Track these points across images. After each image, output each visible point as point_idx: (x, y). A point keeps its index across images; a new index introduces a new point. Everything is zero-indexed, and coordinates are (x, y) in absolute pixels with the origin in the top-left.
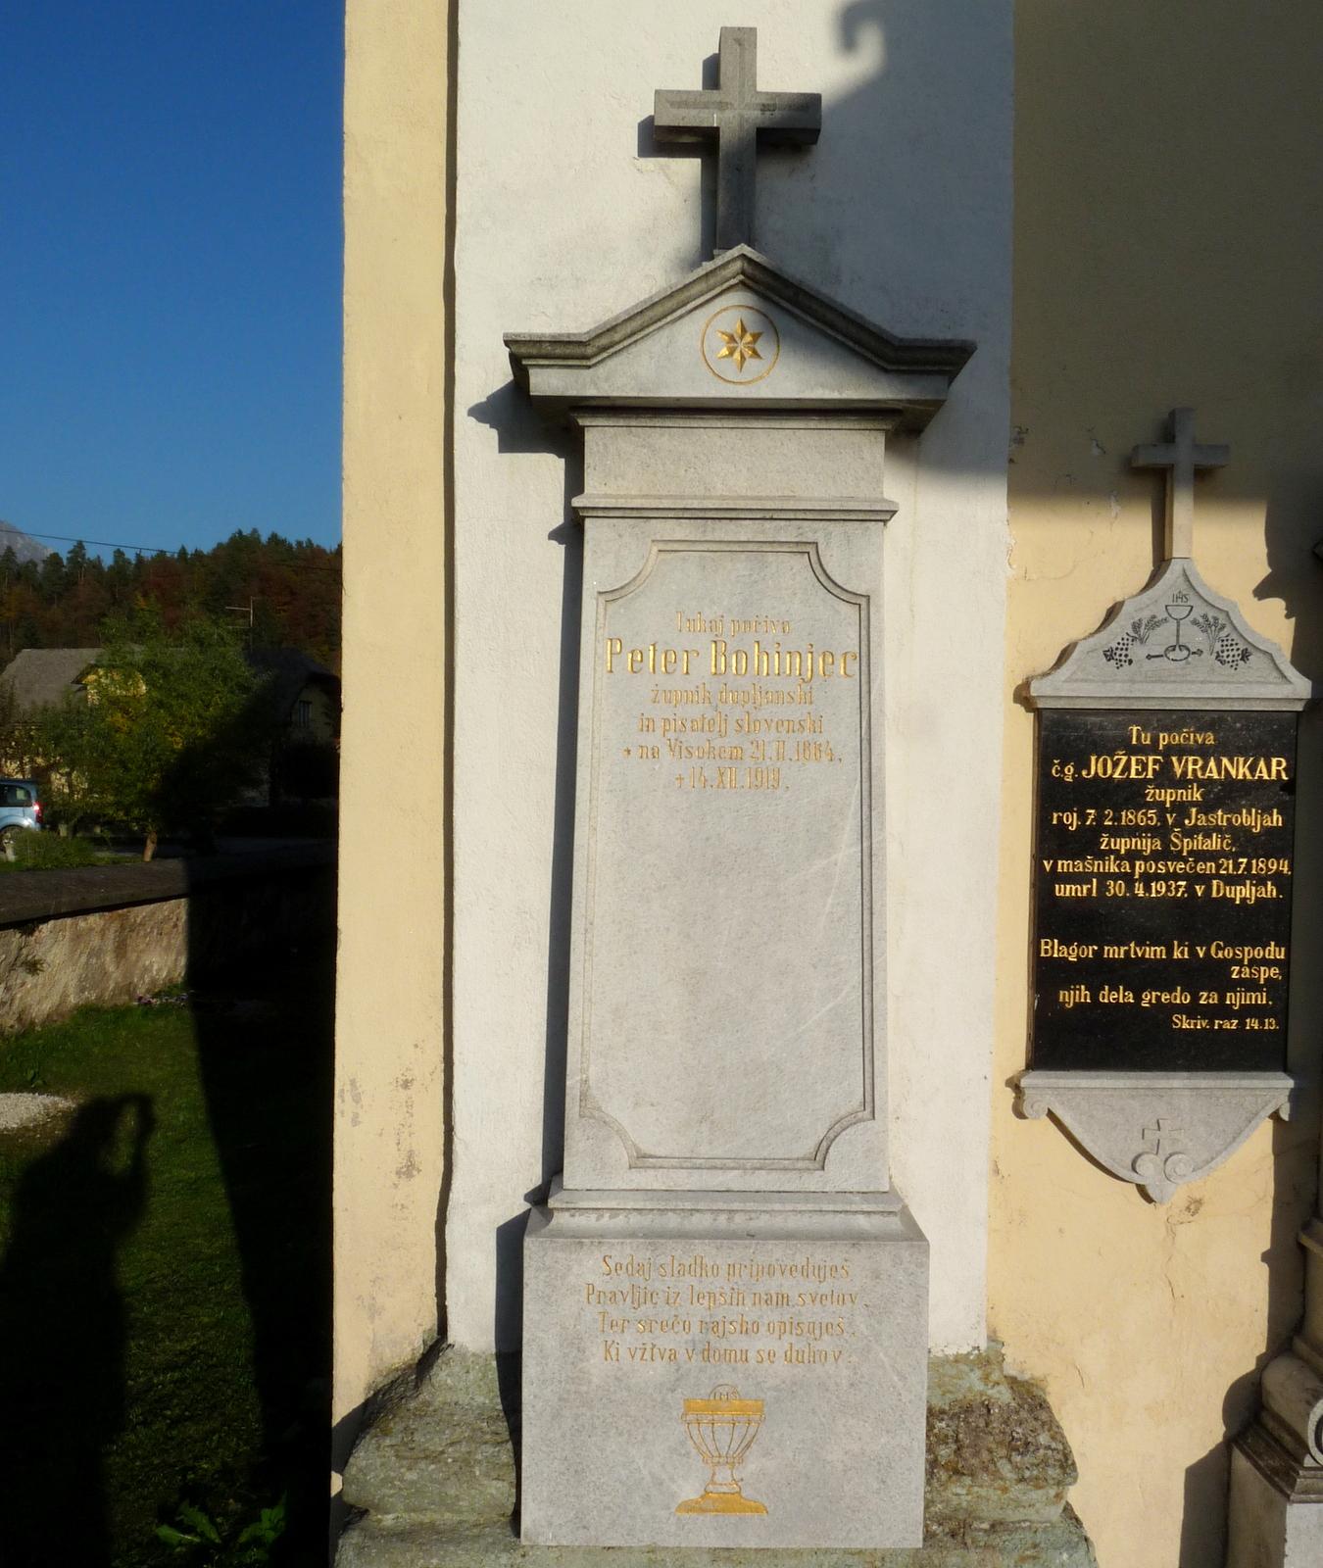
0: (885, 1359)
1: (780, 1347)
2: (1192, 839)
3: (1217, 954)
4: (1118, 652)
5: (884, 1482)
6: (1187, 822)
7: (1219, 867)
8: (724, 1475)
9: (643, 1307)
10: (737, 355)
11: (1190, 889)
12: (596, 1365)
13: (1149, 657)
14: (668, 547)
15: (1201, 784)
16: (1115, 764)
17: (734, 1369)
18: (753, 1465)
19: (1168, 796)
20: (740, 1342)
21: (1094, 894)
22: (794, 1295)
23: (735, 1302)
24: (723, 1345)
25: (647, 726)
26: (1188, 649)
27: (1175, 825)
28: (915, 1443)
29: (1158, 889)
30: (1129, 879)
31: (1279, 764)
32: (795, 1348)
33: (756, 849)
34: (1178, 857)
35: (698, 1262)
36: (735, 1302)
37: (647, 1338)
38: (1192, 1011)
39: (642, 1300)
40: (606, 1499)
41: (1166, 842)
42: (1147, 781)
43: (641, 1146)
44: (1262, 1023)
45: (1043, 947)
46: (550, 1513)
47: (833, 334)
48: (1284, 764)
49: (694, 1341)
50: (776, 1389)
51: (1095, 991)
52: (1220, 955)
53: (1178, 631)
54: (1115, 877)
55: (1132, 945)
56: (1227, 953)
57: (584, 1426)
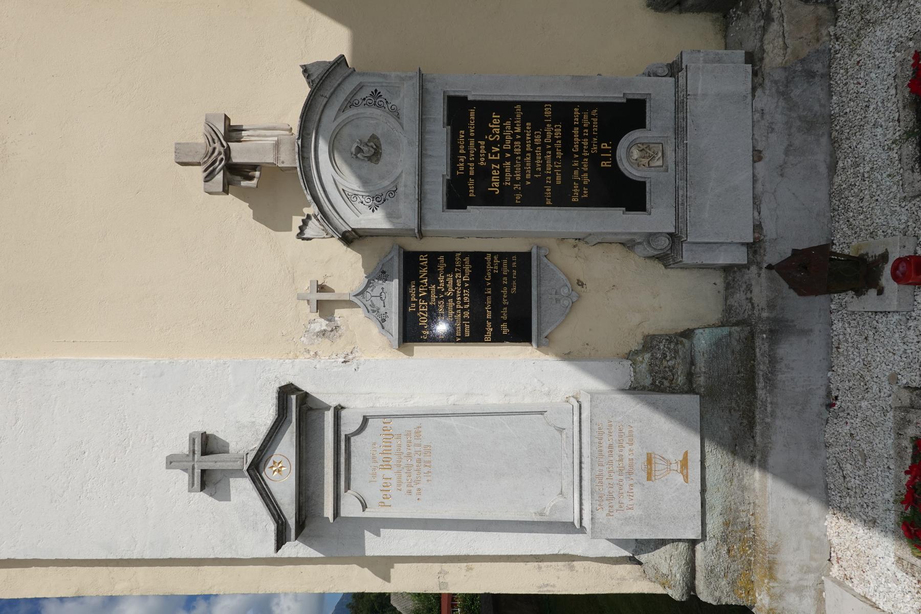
0: (631, 410)
1: (627, 447)
2: (448, 288)
3: (489, 278)
4: (383, 317)
5: (676, 409)
6: (443, 290)
7: (458, 278)
8: (674, 467)
9: (614, 496)
10: (280, 465)
11: (466, 288)
12: (637, 512)
13: (384, 306)
14: (348, 487)
15: (429, 285)
16: (422, 316)
17: (636, 463)
18: (670, 456)
19: (433, 297)
20: (626, 462)
21: (499, 116)
22: (608, 443)
23: (611, 464)
24: (627, 468)
25: (409, 492)
26: (381, 293)
27: (444, 294)
28: (661, 398)
29: (466, 299)
30: (463, 310)
31: (422, 258)
32: (628, 442)
33: (452, 453)
34: (455, 293)
35: (597, 477)
36: (611, 464)
37: (625, 495)
38: (510, 287)
39: (612, 497)
40: (684, 508)
41: (450, 297)
42: (428, 305)
43: (559, 493)
44: (514, 261)
45: (487, 340)
46: (689, 528)
47: (273, 436)
48: (422, 256)
49: (626, 478)
50: (642, 448)
51: (503, 321)
52: (490, 277)
53: (375, 296)
54: (462, 315)
55: (486, 308)
56: (489, 274)
57: (657, 517)
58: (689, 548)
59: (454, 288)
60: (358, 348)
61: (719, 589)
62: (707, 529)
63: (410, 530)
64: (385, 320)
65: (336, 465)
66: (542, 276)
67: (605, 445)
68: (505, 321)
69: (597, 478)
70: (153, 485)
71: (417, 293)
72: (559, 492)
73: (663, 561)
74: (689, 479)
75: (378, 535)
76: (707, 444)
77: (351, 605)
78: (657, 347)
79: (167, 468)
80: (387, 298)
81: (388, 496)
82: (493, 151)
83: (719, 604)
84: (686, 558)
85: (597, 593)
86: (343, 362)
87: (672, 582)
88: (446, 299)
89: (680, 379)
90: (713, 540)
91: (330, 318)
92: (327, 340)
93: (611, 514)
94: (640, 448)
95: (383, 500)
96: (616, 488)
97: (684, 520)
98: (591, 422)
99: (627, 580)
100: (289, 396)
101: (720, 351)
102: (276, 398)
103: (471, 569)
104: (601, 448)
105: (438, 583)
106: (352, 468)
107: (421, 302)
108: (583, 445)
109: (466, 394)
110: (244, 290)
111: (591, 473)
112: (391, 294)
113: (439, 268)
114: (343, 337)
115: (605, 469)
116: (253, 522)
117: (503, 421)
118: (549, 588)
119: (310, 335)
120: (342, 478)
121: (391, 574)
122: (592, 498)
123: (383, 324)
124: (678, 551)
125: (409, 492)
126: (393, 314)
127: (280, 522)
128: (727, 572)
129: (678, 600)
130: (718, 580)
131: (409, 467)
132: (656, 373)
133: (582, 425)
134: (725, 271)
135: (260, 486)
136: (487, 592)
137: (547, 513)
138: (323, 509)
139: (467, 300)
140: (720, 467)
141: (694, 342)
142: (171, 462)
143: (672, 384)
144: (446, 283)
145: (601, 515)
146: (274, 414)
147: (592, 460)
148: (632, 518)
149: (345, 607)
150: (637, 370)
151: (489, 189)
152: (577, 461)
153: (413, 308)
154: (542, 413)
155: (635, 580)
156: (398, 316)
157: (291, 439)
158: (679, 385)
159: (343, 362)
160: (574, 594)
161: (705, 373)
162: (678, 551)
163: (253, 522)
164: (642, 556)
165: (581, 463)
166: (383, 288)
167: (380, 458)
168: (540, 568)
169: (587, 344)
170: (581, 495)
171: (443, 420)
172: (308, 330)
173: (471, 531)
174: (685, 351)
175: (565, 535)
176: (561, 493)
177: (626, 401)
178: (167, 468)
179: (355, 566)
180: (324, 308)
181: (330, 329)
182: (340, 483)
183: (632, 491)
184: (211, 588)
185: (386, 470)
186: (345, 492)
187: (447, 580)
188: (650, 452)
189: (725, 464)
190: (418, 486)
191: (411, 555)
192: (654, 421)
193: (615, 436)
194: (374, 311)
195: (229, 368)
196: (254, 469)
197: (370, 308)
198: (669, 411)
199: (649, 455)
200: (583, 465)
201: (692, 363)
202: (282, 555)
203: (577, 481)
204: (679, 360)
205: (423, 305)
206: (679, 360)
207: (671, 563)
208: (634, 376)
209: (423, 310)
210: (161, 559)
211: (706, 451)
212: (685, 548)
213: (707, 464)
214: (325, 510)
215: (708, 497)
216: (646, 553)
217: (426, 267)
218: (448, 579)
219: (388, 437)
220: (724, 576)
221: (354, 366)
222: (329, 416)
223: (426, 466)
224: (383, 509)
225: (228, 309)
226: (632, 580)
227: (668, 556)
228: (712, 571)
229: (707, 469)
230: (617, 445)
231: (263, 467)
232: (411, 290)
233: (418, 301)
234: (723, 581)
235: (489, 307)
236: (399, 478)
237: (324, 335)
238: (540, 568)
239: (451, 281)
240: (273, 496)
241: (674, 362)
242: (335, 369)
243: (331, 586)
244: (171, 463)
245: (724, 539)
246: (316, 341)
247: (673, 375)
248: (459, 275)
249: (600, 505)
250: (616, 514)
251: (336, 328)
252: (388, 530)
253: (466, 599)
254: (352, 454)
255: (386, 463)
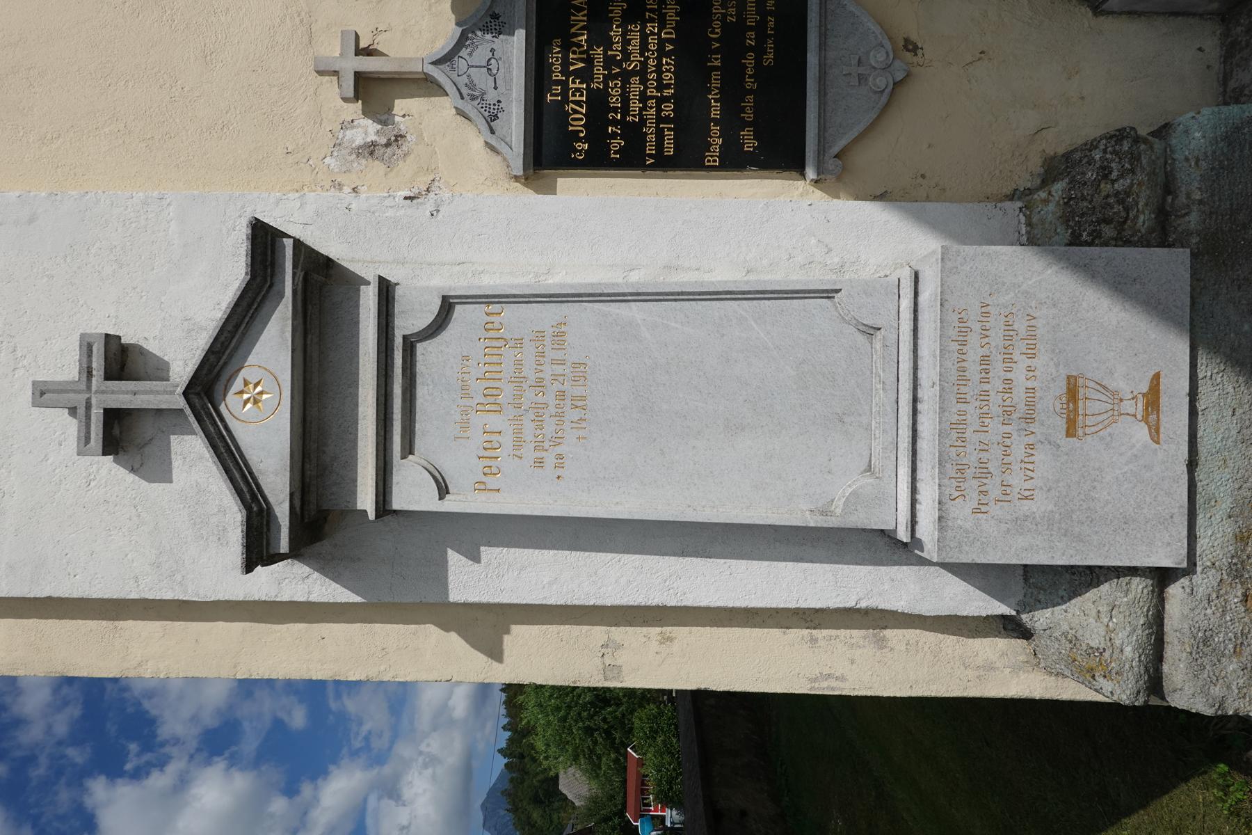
1: (1023, 362)
4: (492, 111)
7: (652, 33)
8: (1128, 406)
9: (991, 470)
10: (259, 389)
11: (668, 55)
12: (1040, 506)
13: (496, 88)
14: (409, 449)
15: (590, 47)
18: (1119, 384)
19: (599, 71)
20: (1019, 396)
22: (981, 352)
23: (987, 398)
24: (1022, 407)
25: (540, 462)
26: (490, 59)
27: (621, 67)
29: (668, 77)
30: (661, 101)
34: (644, 64)
35: (954, 426)
36: (987, 398)
37: (1015, 467)
38: (760, 51)
39: (985, 471)
40: (1148, 499)
41: (634, 73)
45: (712, 164)
50: (1057, 365)
53: (477, 67)
54: (659, 110)
55: (710, 97)
56: (717, 24)
58: (1153, 591)
59: (642, 55)
60: (442, 181)
61: (1221, 681)
62: (1198, 549)
63: (543, 551)
64: (496, 117)
65: (382, 399)
66: (829, 27)
67: (974, 354)
68: (749, 124)
69: (953, 430)
70: (16, 446)
71: (566, 63)
72: (864, 466)
73: (1091, 620)
74: (1161, 435)
75: (476, 558)
76: (1202, 360)
77: (507, 792)
78: (1085, 160)
79: (35, 404)
80: (502, 70)
81: (494, 470)
82: (713, 47)
83: (1220, 712)
84: (1148, 611)
85: (933, 695)
86: (406, 198)
87: (1113, 665)
88: (626, 76)
89: (1142, 218)
90: (1210, 574)
91: (384, 117)
92: (377, 162)
93: (984, 509)
94: (1051, 364)
95: (484, 479)
96: (996, 452)
97: (1149, 525)
98: (941, 305)
99: (998, 668)
100: (278, 239)
101: (1236, 155)
102: (248, 238)
103: (671, 639)
104: (963, 364)
105: (601, 667)
106: (418, 410)
107: (574, 82)
108: (920, 363)
109: (665, 267)
110: (208, 58)
111: (940, 418)
112: (511, 63)
113: (612, 11)
114: (412, 156)
115: (972, 410)
116: (218, 526)
117: (742, 313)
118: (833, 683)
119: (343, 152)
120: (395, 427)
121: (505, 647)
122: (940, 472)
123: (492, 124)
124: (1131, 596)
125: (540, 462)
126: (514, 103)
127: (255, 509)
128: (1242, 643)
129: (1127, 702)
130: (1219, 661)
131: (539, 408)
132: (1083, 215)
133: (920, 318)
134: (1223, 20)
135: (212, 429)
136: (703, 687)
137: (838, 511)
138: (354, 493)
139: (671, 79)
140: (1231, 413)
141: (1174, 142)
142: (43, 393)
143: (1124, 230)
144: (626, 42)
145: (961, 512)
146: (243, 272)
147: (942, 389)
148: (1030, 519)
149: (499, 794)
150: (1034, 220)
151: (709, 64)
152: (905, 397)
153: (556, 95)
154: (829, 294)
155: (1016, 669)
156: (523, 107)
157: (283, 331)
158: (1140, 231)
159: (406, 198)
160: (885, 695)
161: (1201, 202)
162: (1131, 596)
163: (218, 526)
164: (1038, 614)
165: (915, 400)
166: (492, 50)
167: (477, 387)
168: (814, 640)
169: (923, 176)
170: (914, 470)
171: (614, 308)
172: (338, 142)
173: (670, 555)
174: (1153, 157)
175: (871, 567)
176: (869, 468)
177: (1023, 259)
178: (35, 404)
179: (431, 628)
180: (377, 108)
181: (384, 141)
182: (391, 438)
183: (1031, 459)
184: (140, 665)
185: (492, 415)
186: (402, 458)
187: (619, 662)
188: (1074, 374)
189: (1241, 405)
190: (559, 450)
191: (544, 602)
192: (1085, 305)
193: (996, 338)
194: (473, 98)
195: (171, 208)
196: (203, 395)
197: (465, 91)
198: (1120, 283)
199: (1072, 381)
200: (919, 406)
201: (1168, 188)
202: (276, 596)
203: (906, 445)
204: (1141, 176)
205: (578, 90)
206: (1141, 176)
207: (1110, 624)
208: (1028, 233)
209: (577, 98)
210: (29, 599)
211: (1200, 376)
212: (1145, 591)
213: (1201, 405)
214: (359, 495)
215: (1201, 477)
216: (1047, 608)
217: (584, 9)
218: (623, 658)
219: (495, 343)
220: (1235, 652)
221: (429, 206)
222: (369, 299)
223: (577, 407)
224: (483, 496)
225: (177, 99)
226: (1009, 670)
227: (1104, 609)
228: (1206, 641)
229: (1200, 417)
230: (1000, 357)
231: (222, 393)
232: (552, 58)
233: (567, 80)
234: (1231, 662)
235: (716, 94)
236: (518, 431)
237: (371, 153)
238: (814, 640)
239: (636, 41)
240: (242, 455)
241: (1128, 181)
242: (390, 213)
243: (382, 668)
244: (42, 394)
245: (1236, 570)
246: (355, 165)
247: (1127, 210)
248: (654, 27)
249: (958, 488)
250: (995, 510)
251: (396, 140)
252: (497, 550)
253: (661, 781)
254: (419, 380)
255: (491, 399)
